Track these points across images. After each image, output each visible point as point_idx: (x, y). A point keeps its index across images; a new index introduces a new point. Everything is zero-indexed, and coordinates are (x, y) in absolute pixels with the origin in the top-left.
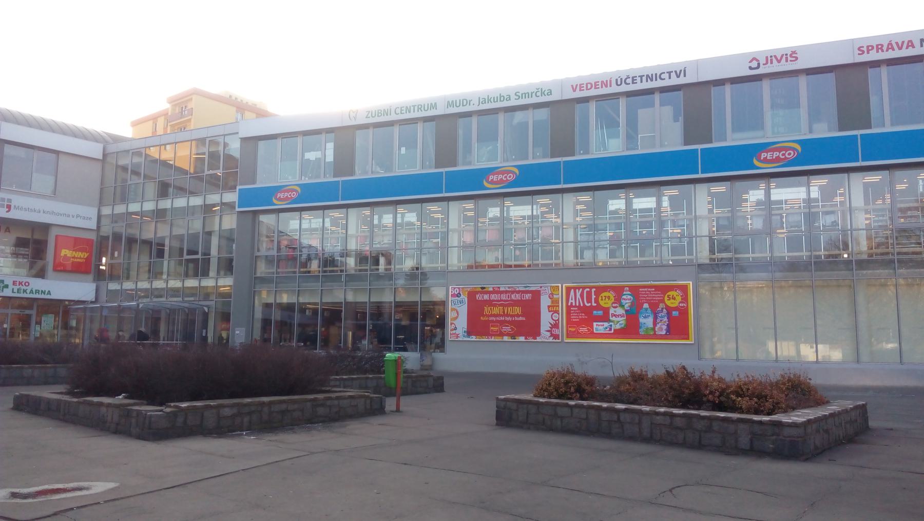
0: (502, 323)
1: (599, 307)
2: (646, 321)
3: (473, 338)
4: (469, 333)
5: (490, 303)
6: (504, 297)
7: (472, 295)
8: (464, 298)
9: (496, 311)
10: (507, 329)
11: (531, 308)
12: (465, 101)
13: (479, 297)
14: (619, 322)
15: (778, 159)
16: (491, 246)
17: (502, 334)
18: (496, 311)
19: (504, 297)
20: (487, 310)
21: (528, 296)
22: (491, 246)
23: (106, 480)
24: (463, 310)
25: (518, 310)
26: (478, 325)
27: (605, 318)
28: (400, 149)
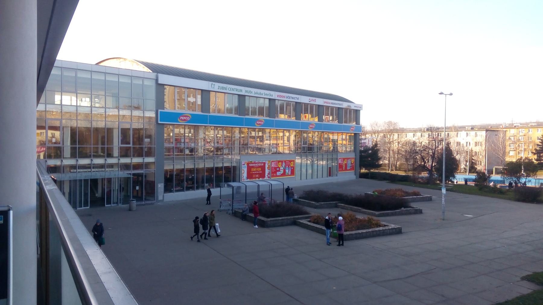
0: (256, 174)
1: (278, 167)
2: (287, 171)
3: (249, 180)
4: (248, 178)
5: (253, 167)
6: (257, 165)
7: (248, 164)
8: (246, 165)
9: (255, 170)
10: (257, 176)
11: (263, 168)
12: (37, 225)
13: (250, 165)
14: (282, 172)
15: (185, 120)
16: (219, 122)
17: (256, 178)
18: (255, 170)
19: (257, 165)
20: (252, 170)
21: (262, 164)
22: (219, 122)
23: (61, 249)
24: (246, 170)
25: (260, 169)
26: (250, 176)
27: (279, 171)
28: (134, 188)
